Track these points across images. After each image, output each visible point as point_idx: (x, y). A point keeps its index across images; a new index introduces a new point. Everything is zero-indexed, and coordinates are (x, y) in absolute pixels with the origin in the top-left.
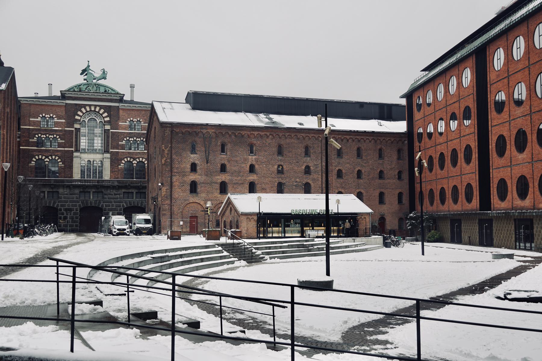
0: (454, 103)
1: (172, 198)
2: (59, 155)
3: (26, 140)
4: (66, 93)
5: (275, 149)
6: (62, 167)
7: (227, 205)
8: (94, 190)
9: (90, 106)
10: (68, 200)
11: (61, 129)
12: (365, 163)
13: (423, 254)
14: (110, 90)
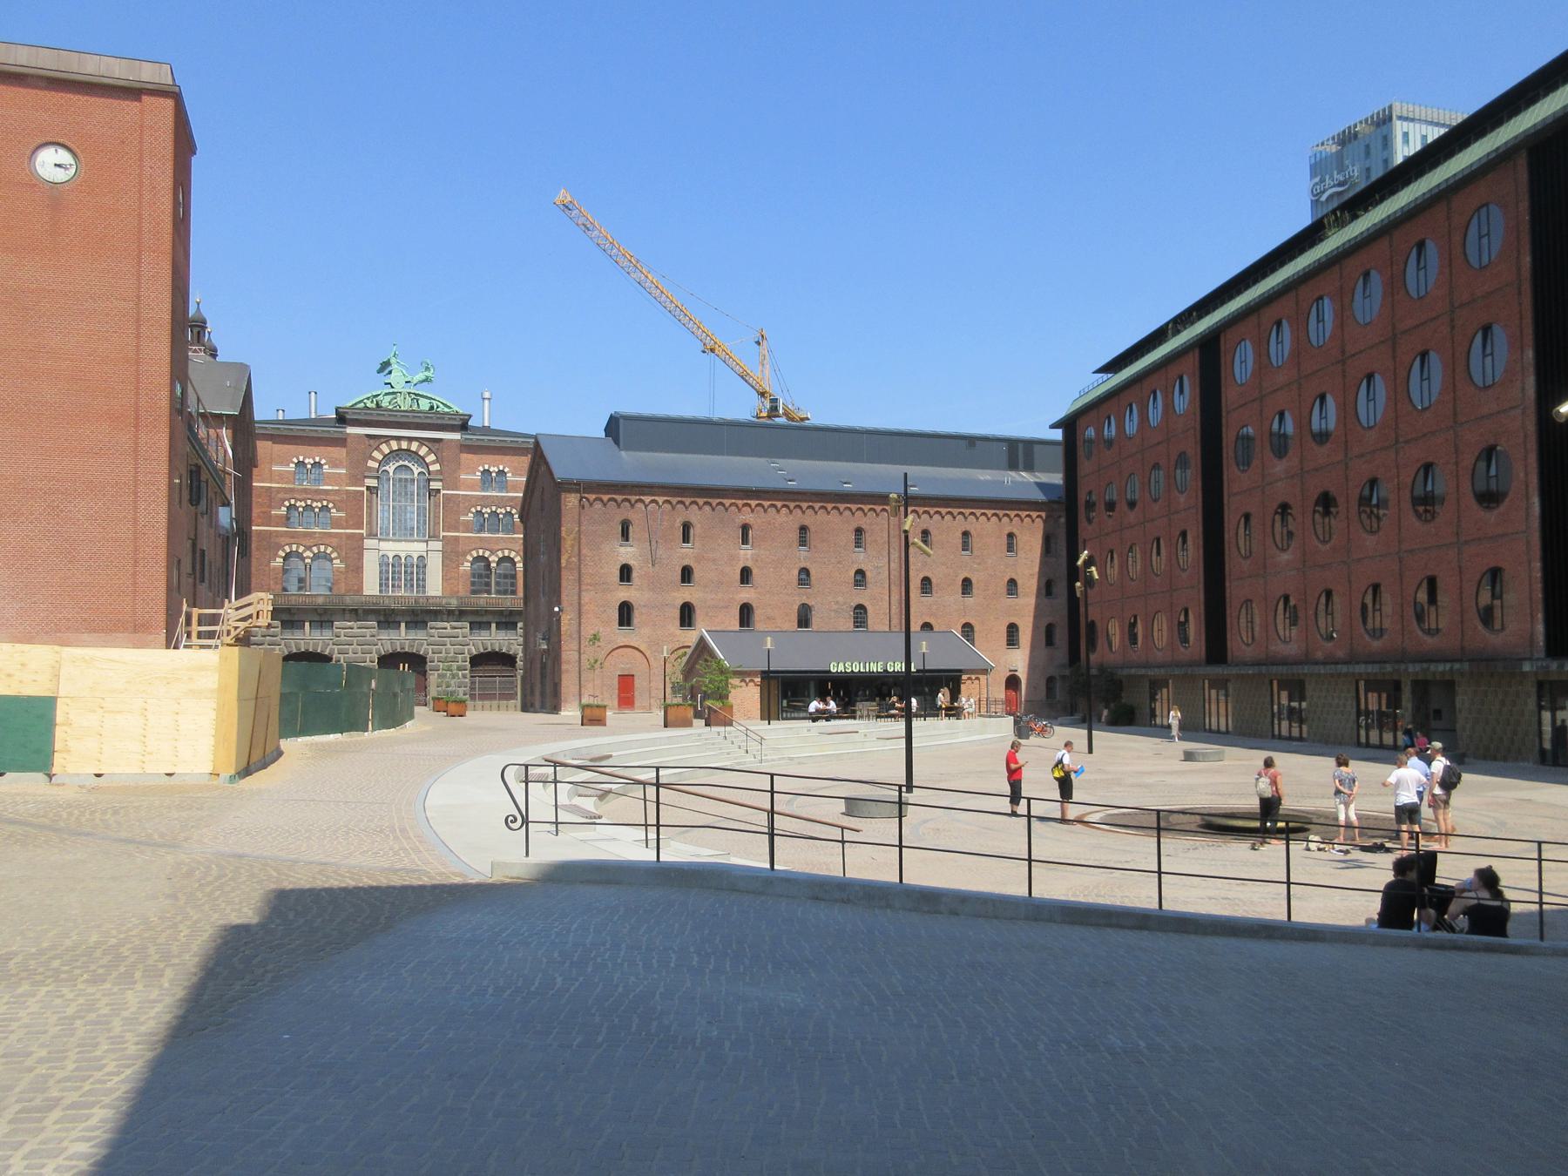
0: (1159, 443)
1: (582, 638)
2: (334, 544)
3: (264, 513)
4: (347, 413)
5: (795, 535)
6: (341, 570)
7: (697, 652)
8: (409, 619)
9: (398, 439)
10: (442, 649)
11: (337, 488)
12: (979, 564)
13: (1090, 751)
14: (441, 405)
